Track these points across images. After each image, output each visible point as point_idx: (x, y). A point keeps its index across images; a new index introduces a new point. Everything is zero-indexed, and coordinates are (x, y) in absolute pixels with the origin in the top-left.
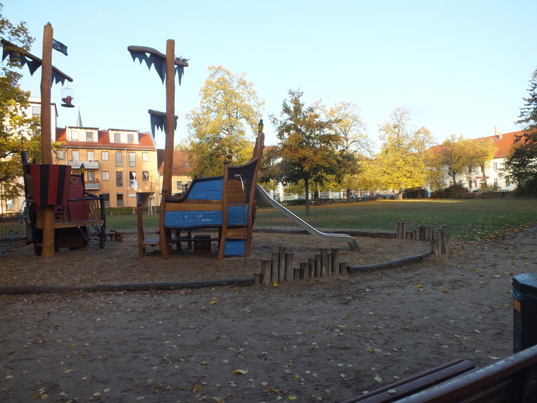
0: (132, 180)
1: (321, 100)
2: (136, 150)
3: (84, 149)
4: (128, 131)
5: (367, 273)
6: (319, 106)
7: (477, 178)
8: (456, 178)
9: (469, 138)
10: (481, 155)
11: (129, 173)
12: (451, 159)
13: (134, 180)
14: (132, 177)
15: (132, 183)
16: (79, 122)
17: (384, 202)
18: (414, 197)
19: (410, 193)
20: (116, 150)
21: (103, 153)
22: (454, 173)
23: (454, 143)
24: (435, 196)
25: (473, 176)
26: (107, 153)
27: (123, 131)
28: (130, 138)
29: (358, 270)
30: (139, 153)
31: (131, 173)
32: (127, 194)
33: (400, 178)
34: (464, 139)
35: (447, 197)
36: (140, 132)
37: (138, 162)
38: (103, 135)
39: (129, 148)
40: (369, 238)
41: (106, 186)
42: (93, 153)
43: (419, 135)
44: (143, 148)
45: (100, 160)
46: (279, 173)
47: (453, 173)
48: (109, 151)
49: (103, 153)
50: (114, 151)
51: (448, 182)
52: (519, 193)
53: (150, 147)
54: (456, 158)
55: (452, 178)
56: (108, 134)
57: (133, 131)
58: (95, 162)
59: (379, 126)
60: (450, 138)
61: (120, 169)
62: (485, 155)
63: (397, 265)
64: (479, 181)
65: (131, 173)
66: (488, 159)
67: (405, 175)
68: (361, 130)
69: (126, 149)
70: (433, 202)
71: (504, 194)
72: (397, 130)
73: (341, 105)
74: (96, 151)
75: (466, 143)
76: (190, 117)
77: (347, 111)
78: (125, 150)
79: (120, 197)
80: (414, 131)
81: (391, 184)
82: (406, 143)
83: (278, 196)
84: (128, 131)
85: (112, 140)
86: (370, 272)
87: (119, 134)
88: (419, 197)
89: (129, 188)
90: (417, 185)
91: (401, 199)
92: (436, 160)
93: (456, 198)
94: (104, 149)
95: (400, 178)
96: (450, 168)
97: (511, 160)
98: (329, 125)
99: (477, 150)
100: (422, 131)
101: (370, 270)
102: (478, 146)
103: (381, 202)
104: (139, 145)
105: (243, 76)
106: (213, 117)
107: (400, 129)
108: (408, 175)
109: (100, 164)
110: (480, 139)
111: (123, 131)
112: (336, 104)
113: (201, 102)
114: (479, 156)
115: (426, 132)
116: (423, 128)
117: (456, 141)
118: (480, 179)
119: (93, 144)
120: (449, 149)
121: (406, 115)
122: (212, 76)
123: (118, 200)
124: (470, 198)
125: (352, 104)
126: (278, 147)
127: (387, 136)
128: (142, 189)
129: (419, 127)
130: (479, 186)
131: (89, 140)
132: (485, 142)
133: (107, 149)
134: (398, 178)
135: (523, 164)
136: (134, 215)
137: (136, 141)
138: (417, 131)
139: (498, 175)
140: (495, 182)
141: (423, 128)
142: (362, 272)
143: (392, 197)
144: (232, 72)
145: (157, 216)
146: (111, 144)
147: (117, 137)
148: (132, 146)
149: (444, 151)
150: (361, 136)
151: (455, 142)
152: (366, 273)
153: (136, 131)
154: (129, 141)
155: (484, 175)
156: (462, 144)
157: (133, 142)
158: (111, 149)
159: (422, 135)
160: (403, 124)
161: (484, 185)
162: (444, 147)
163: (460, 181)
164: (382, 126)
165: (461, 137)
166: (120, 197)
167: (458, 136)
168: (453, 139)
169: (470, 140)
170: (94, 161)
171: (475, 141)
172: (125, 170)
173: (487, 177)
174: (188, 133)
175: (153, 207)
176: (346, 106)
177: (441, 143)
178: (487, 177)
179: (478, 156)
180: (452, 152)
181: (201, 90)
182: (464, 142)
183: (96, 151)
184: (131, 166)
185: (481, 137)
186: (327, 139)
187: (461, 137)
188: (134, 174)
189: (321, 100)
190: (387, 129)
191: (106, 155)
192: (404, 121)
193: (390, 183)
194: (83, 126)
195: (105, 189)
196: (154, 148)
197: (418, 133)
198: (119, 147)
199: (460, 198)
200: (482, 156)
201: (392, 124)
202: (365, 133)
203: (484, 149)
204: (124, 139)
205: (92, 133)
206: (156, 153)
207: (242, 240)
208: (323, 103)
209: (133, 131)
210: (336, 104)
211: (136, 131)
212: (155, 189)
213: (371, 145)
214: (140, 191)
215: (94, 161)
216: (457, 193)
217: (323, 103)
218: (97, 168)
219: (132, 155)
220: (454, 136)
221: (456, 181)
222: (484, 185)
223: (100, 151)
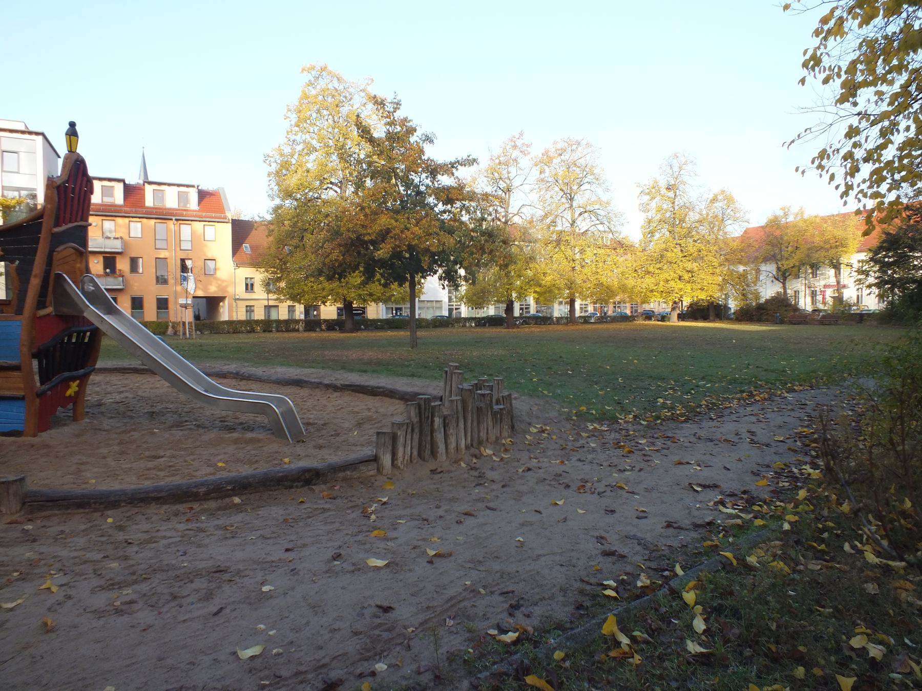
0: (185, 274)
1: (521, 134)
2: (192, 221)
3: (96, 215)
4: (179, 185)
5: (87, 510)
6: (518, 144)
7: (825, 286)
8: (787, 285)
9: (814, 214)
10: (834, 245)
11: (179, 262)
12: (781, 250)
13: (190, 274)
14: (184, 268)
15: (185, 279)
16: (142, 174)
17: (646, 325)
18: (705, 318)
19: (698, 311)
20: (156, 218)
21: (132, 224)
22: (785, 278)
23: (787, 223)
24: (745, 315)
25: (819, 284)
26: (139, 225)
27: (169, 185)
28: (182, 197)
29: (50, 504)
30: (198, 226)
31: (183, 261)
32: (176, 298)
33: (672, 283)
34: (806, 216)
35: (759, 321)
36: (200, 188)
37: (198, 241)
38: (130, 191)
39: (180, 216)
40: (397, 401)
41: (136, 284)
42: (113, 223)
43: (715, 205)
44: (205, 217)
45: (126, 237)
46: (336, 260)
47: (783, 276)
48: (144, 220)
49: (132, 224)
50: (153, 222)
51: (768, 290)
52: (887, 318)
53: (218, 215)
54: (790, 248)
55: (781, 285)
56: (144, 190)
57: (188, 186)
58: (116, 241)
59: (639, 186)
60: (780, 213)
61: (163, 254)
62: (842, 246)
63: (207, 493)
64: (829, 293)
65: (183, 261)
66: (846, 252)
67: (680, 278)
68: (600, 191)
69: (174, 218)
70: (727, 329)
71: (862, 318)
72: (671, 194)
73: (566, 144)
74: (120, 221)
75: (810, 222)
76: (273, 160)
77: (575, 156)
78: (171, 219)
79: (163, 304)
80: (705, 196)
81: (655, 293)
82: (693, 216)
83: (456, 309)
84: (179, 185)
85: (149, 202)
86: (96, 510)
87: (113, 187)
88: (711, 318)
89: (179, 288)
90: (702, 296)
91: (674, 322)
92: (742, 250)
93: (775, 323)
94: (133, 217)
95: (672, 283)
96: (778, 269)
97: (876, 253)
98: (449, 168)
99: (828, 236)
100: (720, 197)
101: (101, 504)
102: (829, 228)
103: (640, 325)
104: (199, 211)
105: (368, 84)
106: (312, 162)
107: (678, 193)
108: (686, 276)
109: (125, 244)
110: (833, 215)
111: (169, 185)
112: (555, 143)
113: (288, 132)
114: (831, 247)
115: (729, 200)
116: (723, 192)
117: (791, 219)
118: (831, 290)
119: (113, 208)
120: (778, 233)
121: (689, 167)
122: (310, 84)
123: (159, 308)
124: (799, 323)
125: (583, 143)
126: (348, 211)
127: (653, 204)
128: (204, 290)
129: (716, 190)
130: (830, 301)
131: (107, 200)
132: (844, 221)
133: (140, 218)
134: (667, 281)
135: (902, 261)
136: (168, 335)
137: (193, 203)
138: (711, 196)
139: (855, 282)
140: (858, 296)
141: (723, 192)
142: (68, 508)
143: (663, 318)
144: (345, 77)
145: (196, 338)
146: (148, 208)
147: (157, 194)
148: (185, 213)
149: (768, 236)
150: (599, 201)
151: (788, 220)
152: (82, 510)
153: (193, 186)
154: (182, 204)
155: (838, 282)
156: (801, 224)
157: (188, 206)
158: (147, 218)
159: (720, 204)
160: (684, 183)
161: (839, 300)
162: (767, 230)
163: (795, 292)
164: (645, 185)
165: (801, 212)
166: (163, 304)
167: (795, 210)
168: (786, 215)
169: (816, 217)
170: (115, 238)
171: (824, 219)
172: (172, 257)
173: (844, 286)
174: (268, 188)
175: (174, 323)
176: (574, 147)
177: (763, 222)
178: (844, 286)
179: (828, 246)
180: (782, 239)
181: (289, 110)
182: (805, 221)
183: (119, 220)
184: (182, 248)
185: (835, 213)
186: (448, 196)
187: (801, 212)
188: (189, 263)
189: (521, 134)
190: (652, 191)
191: (136, 228)
192: (685, 178)
193: (652, 291)
194: (150, 179)
195: (136, 288)
196: (225, 218)
197: (714, 200)
198: (162, 215)
199: (782, 322)
200: (836, 247)
201: (663, 184)
202: (604, 198)
203: (839, 233)
204: (171, 200)
205: (187, 193)
206: (229, 227)
207: (22, 398)
208: (526, 139)
209: (188, 186)
210: (555, 143)
211: (193, 186)
212: (227, 292)
213: (614, 219)
214: (200, 293)
215: (115, 238)
216: (776, 313)
217: (526, 139)
218: (120, 251)
219: (186, 231)
220: (787, 210)
221: (789, 291)
222: (839, 300)
223: (127, 220)
